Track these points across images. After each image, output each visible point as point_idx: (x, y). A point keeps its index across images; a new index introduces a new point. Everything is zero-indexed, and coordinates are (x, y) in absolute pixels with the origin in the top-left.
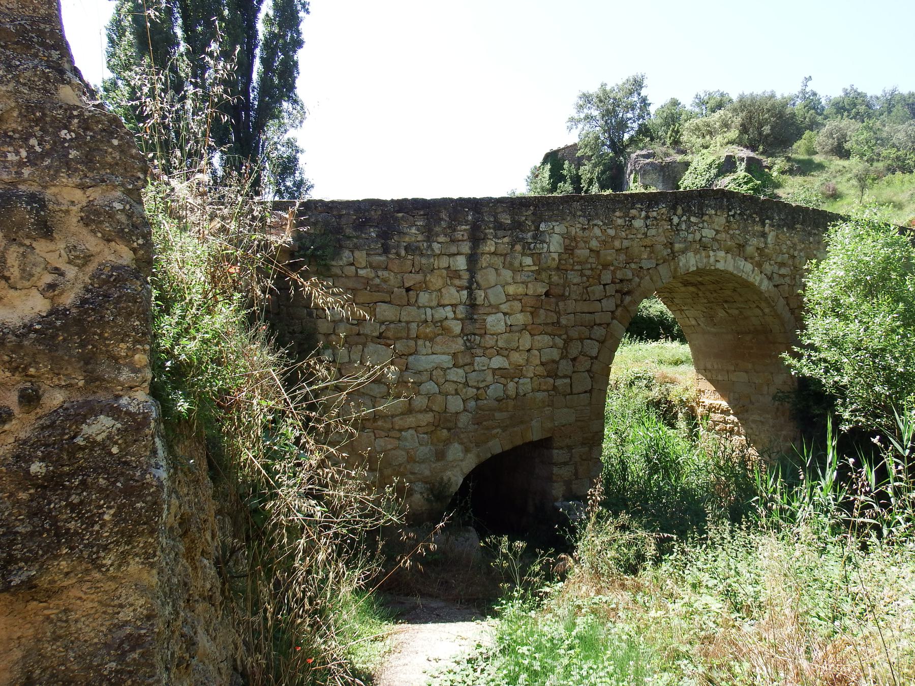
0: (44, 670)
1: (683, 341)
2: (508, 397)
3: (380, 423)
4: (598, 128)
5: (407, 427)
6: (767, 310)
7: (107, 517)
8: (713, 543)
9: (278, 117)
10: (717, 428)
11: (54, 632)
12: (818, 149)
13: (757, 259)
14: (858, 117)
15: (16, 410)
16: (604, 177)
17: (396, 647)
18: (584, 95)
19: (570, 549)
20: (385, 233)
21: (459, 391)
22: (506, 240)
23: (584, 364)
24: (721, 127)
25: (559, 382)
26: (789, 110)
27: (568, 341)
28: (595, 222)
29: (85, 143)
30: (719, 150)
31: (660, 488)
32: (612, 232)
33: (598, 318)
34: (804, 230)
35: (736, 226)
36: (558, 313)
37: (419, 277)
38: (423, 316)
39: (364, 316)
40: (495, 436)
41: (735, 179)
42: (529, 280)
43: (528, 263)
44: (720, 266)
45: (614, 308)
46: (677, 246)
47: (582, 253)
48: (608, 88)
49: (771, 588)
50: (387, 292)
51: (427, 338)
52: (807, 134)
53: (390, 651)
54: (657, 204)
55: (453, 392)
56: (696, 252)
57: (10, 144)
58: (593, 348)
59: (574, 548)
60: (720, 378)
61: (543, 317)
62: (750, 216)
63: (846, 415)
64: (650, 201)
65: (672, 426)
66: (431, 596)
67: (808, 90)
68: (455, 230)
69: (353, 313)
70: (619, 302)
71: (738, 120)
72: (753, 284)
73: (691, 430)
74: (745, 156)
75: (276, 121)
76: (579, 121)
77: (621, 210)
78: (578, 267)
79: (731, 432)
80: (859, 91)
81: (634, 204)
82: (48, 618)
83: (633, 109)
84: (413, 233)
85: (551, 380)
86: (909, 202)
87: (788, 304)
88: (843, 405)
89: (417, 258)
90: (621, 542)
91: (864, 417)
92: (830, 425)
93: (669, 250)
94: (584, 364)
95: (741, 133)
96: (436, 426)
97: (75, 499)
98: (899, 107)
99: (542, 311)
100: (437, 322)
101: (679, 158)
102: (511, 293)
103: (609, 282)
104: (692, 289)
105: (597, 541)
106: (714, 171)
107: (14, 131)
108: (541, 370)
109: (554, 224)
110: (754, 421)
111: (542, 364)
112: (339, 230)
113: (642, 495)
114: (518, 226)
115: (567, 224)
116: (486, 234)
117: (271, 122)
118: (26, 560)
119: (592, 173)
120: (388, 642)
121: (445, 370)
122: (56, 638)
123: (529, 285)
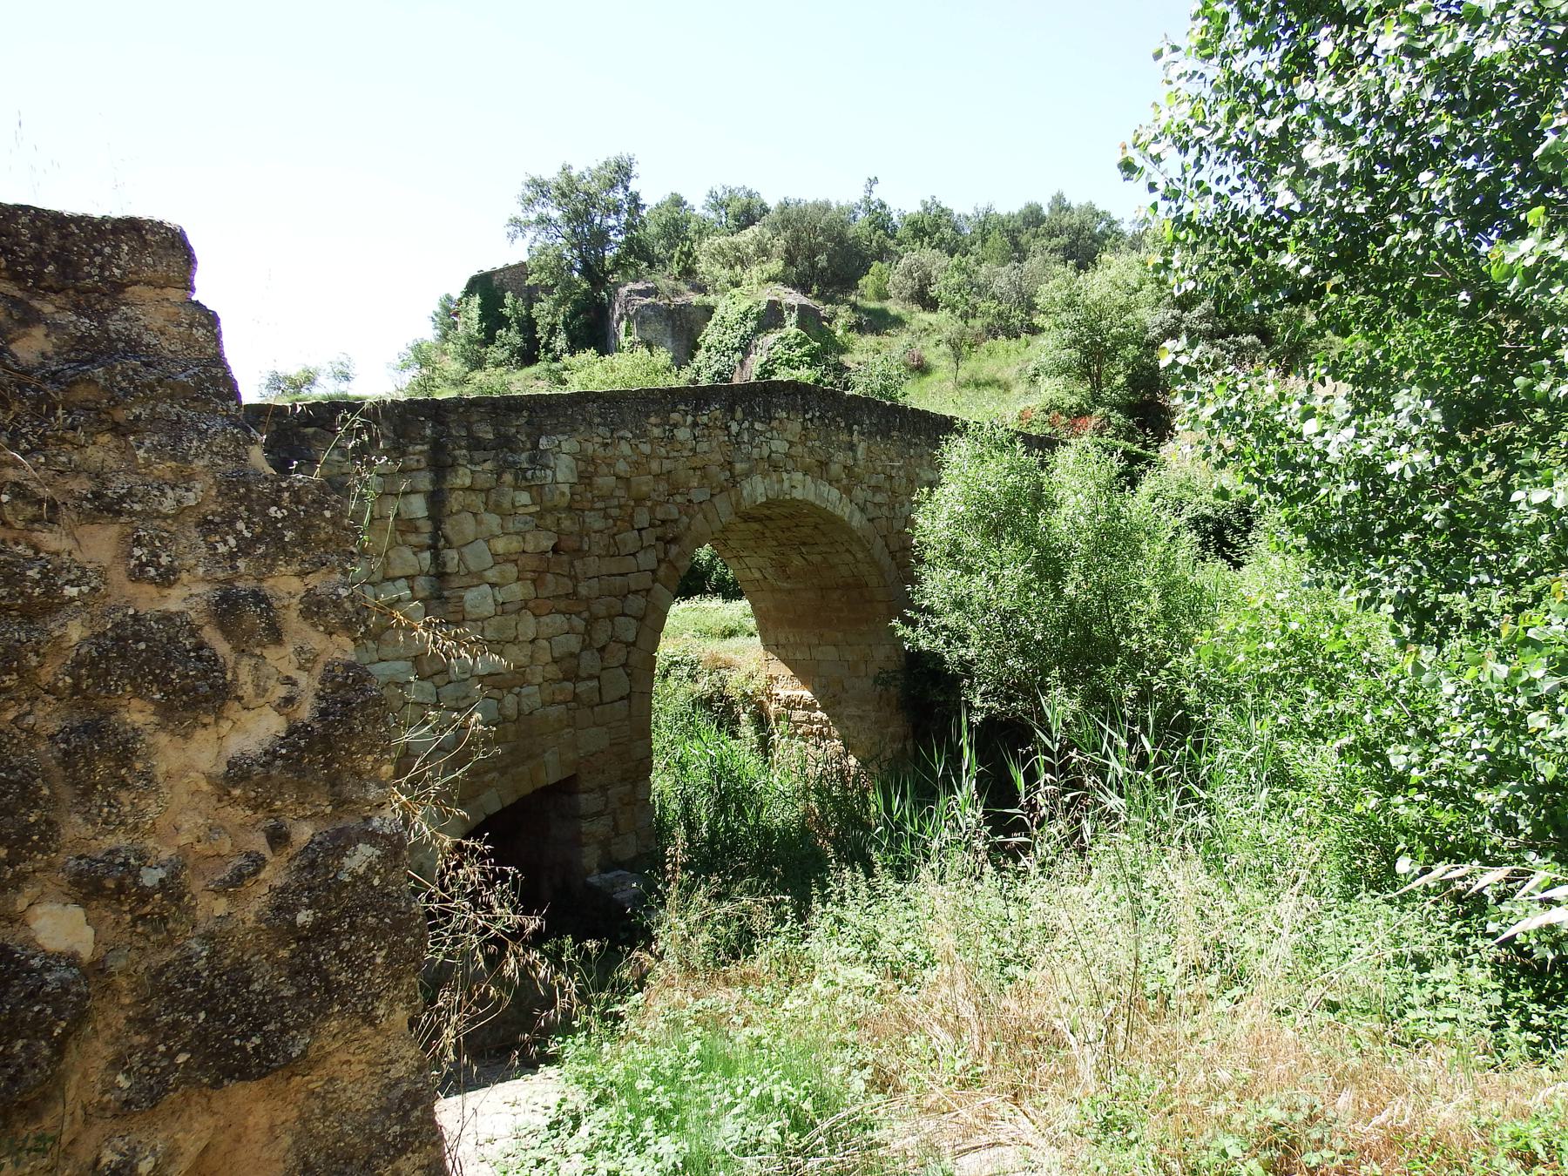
0: (318, 1151)
6: (860, 556)
7: (379, 960)
11: (324, 1108)
12: (893, 292)
13: (845, 482)
15: (268, 854)
16: (576, 323)
18: (534, 181)
22: (488, 466)
23: (617, 654)
25: (582, 687)
26: (850, 233)
27: (592, 621)
28: (621, 433)
29: (300, 521)
30: (759, 288)
36: (574, 578)
40: (488, 786)
42: (527, 528)
44: (798, 494)
45: (654, 566)
46: (739, 467)
47: (605, 482)
48: (574, 173)
52: (876, 266)
56: (765, 475)
57: (216, 532)
60: (799, 656)
61: (551, 587)
62: (833, 419)
64: (698, 399)
67: (873, 198)
70: (662, 556)
71: (780, 243)
74: (795, 303)
76: (528, 225)
77: (657, 415)
81: (675, 405)
82: (313, 1092)
83: (617, 213)
85: (569, 685)
87: (887, 545)
94: (617, 654)
95: (786, 265)
97: (345, 946)
99: (549, 577)
101: (695, 299)
102: (500, 551)
104: (756, 526)
105: (680, 926)
106: (751, 324)
107: (213, 514)
108: (553, 671)
109: (561, 437)
110: (850, 717)
111: (555, 661)
114: (505, 443)
116: (455, 458)
118: (297, 1027)
119: (554, 315)
122: (327, 1113)
123: (528, 537)
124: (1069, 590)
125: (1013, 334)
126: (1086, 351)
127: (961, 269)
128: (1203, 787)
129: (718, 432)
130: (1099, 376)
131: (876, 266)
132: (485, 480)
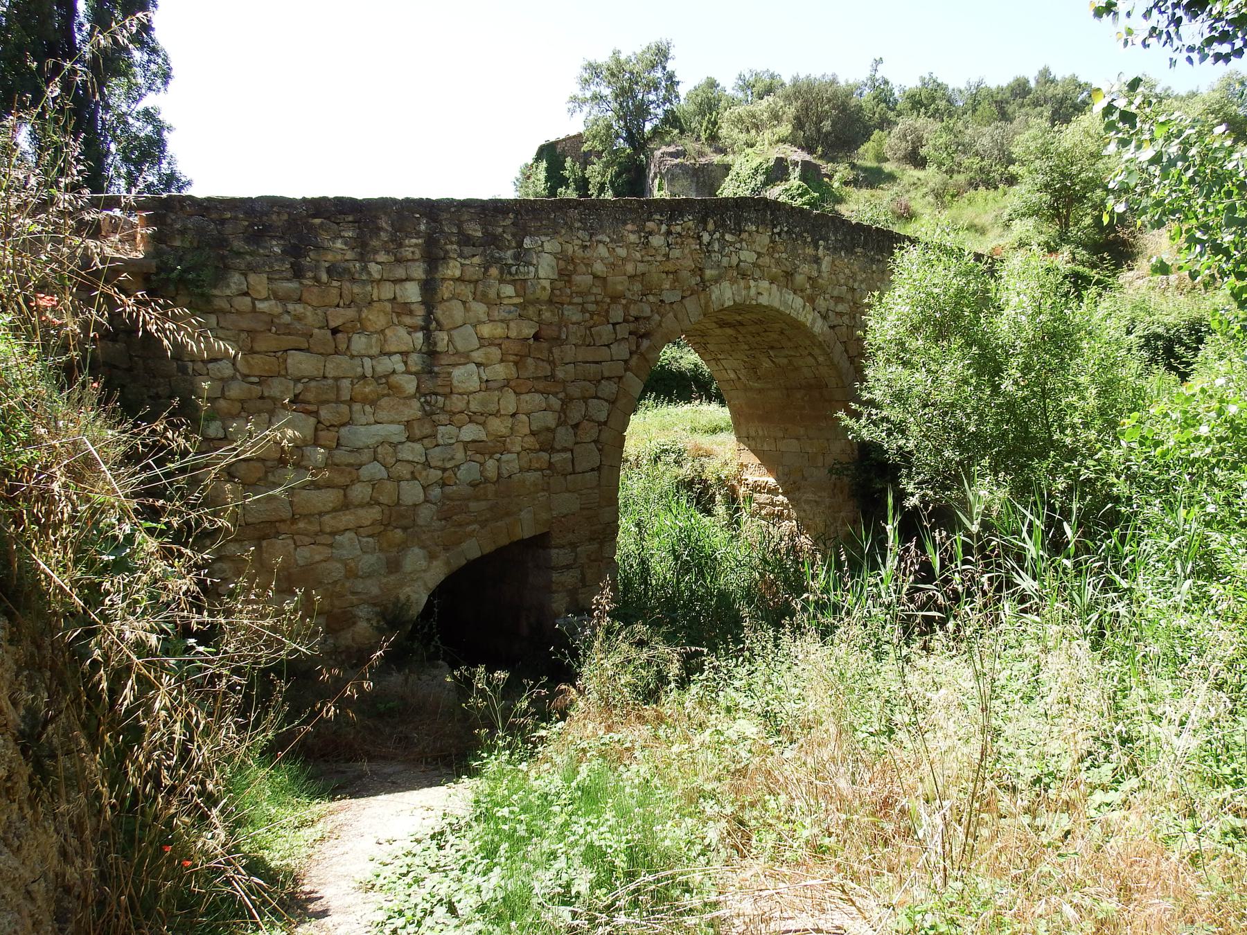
1: (722, 403)
2: (487, 480)
3: (301, 525)
4: (610, 113)
5: (342, 528)
6: (821, 359)
8: (752, 655)
9: (125, 75)
10: (763, 512)
14: (936, 115)
17: (331, 832)
18: (590, 64)
19: (571, 677)
20: (295, 247)
21: (417, 474)
22: (476, 260)
24: (770, 119)
25: (556, 458)
27: (565, 403)
28: (599, 237)
30: (767, 149)
31: (693, 592)
32: (622, 252)
33: (606, 369)
34: (865, 255)
35: (782, 248)
36: (552, 363)
37: (351, 313)
38: (359, 370)
39: (226, 349)
40: (470, 535)
41: (786, 190)
42: (511, 316)
43: (508, 294)
44: (764, 300)
45: (627, 356)
46: (709, 273)
47: (582, 279)
48: (623, 57)
49: (817, 702)
50: (303, 335)
51: (365, 401)
52: (877, 133)
53: (323, 839)
54: (682, 215)
55: (408, 476)
56: (733, 281)
58: (600, 410)
59: (579, 675)
60: (766, 448)
61: (532, 368)
63: (910, 488)
64: (673, 211)
65: (709, 512)
66: (384, 758)
67: (878, 76)
68: (400, 245)
69: (209, 347)
70: (634, 348)
71: (791, 111)
72: (804, 325)
73: (731, 516)
74: (799, 159)
75: (124, 80)
76: (585, 101)
77: (633, 223)
78: (577, 300)
79: (780, 516)
80: (939, 81)
81: (651, 214)
83: (656, 89)
84: (339, 249)
85: (545, 456)
86: (993, 225)
88: (909, 476)
89: (347, 285)
90: (637, 663)
91: (932, 489)
92: (890, 501)
93: (698, 278)
96: (385, 524)
98: (985, 104)
99: (530, 360)
100: (380, 378)
101: (717, 159)
103: (620, 320)
104: (729, 331)
105: (606, 665)
106: (761, 178)
108: (531, 442)
109: (543, 238)
110: (807, 502)
111: (533, 433)
112: (222, 242)
113: (670, 605)
115: (561, 240)
116: (447, 252)
117: (115, 81)
119: (603, 176)
120: (319, 826)
121: (395, 446)
123: (512, 324)
124: (1007, 385)
125: (990, 184)
126: (1058, 194)
127: (948, 130)
128: (1125, 576)
129: (691, 240)
130: (1067, 217)
131: (877, 133)
132: (473, 272)
